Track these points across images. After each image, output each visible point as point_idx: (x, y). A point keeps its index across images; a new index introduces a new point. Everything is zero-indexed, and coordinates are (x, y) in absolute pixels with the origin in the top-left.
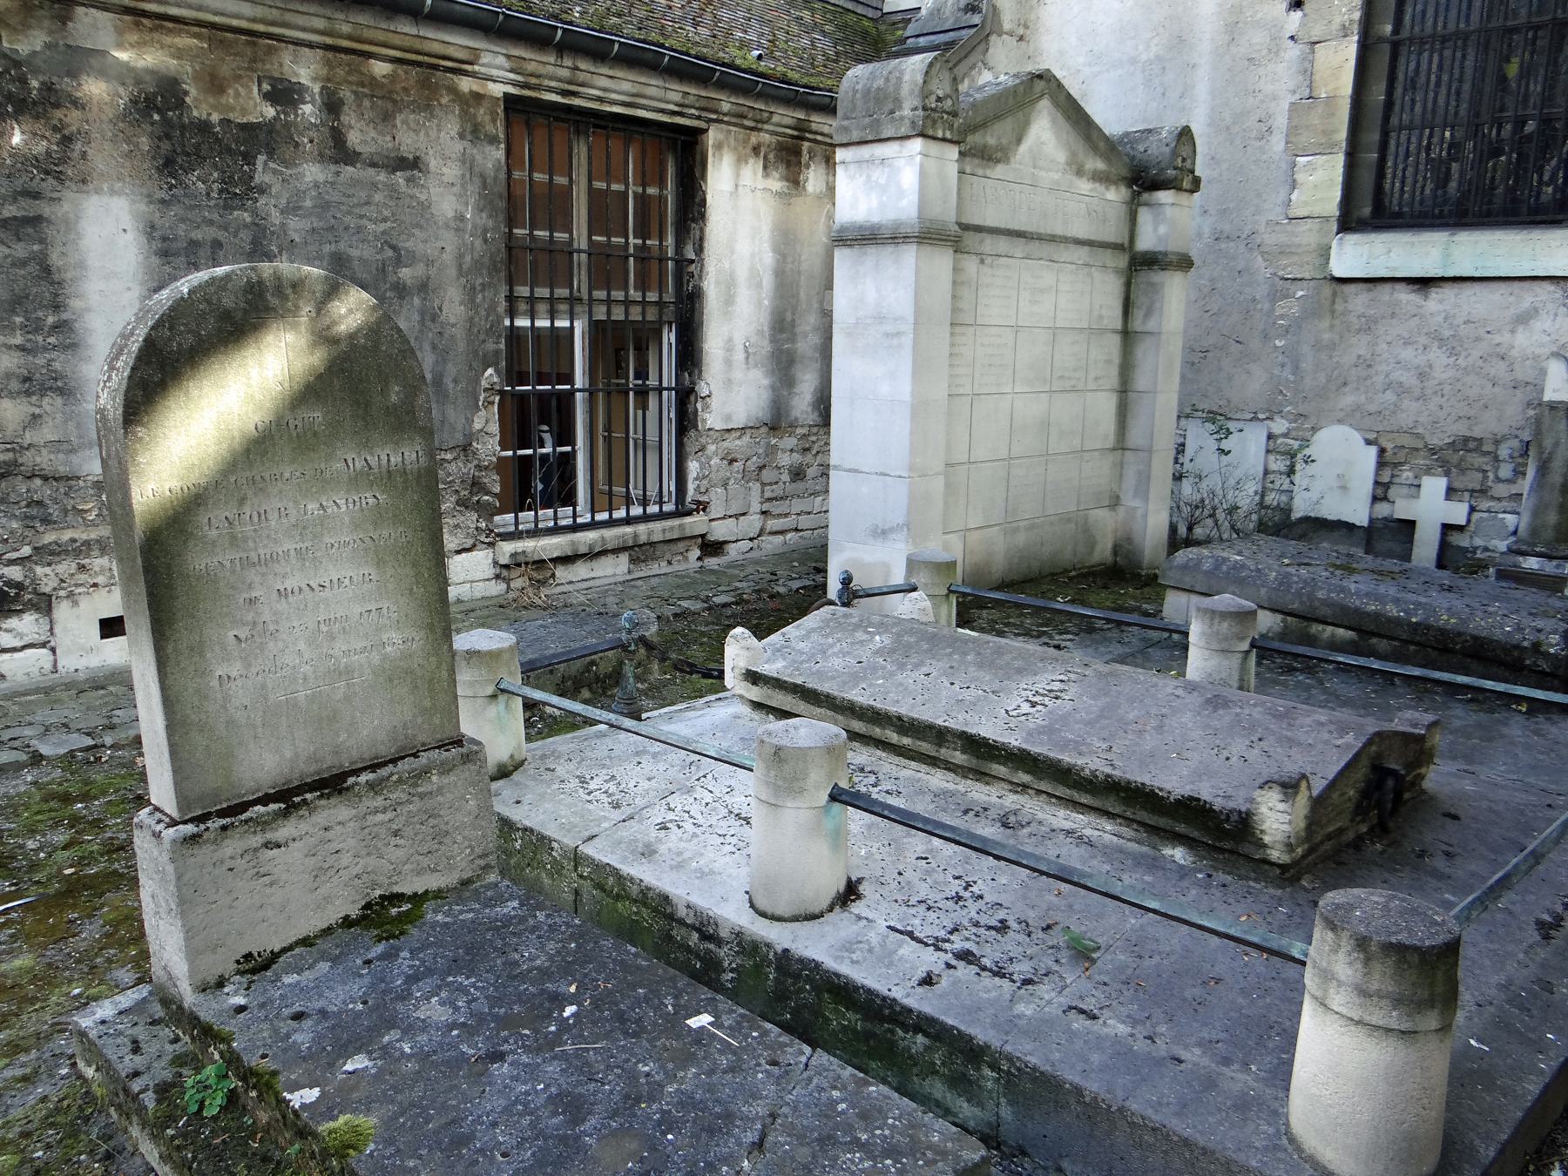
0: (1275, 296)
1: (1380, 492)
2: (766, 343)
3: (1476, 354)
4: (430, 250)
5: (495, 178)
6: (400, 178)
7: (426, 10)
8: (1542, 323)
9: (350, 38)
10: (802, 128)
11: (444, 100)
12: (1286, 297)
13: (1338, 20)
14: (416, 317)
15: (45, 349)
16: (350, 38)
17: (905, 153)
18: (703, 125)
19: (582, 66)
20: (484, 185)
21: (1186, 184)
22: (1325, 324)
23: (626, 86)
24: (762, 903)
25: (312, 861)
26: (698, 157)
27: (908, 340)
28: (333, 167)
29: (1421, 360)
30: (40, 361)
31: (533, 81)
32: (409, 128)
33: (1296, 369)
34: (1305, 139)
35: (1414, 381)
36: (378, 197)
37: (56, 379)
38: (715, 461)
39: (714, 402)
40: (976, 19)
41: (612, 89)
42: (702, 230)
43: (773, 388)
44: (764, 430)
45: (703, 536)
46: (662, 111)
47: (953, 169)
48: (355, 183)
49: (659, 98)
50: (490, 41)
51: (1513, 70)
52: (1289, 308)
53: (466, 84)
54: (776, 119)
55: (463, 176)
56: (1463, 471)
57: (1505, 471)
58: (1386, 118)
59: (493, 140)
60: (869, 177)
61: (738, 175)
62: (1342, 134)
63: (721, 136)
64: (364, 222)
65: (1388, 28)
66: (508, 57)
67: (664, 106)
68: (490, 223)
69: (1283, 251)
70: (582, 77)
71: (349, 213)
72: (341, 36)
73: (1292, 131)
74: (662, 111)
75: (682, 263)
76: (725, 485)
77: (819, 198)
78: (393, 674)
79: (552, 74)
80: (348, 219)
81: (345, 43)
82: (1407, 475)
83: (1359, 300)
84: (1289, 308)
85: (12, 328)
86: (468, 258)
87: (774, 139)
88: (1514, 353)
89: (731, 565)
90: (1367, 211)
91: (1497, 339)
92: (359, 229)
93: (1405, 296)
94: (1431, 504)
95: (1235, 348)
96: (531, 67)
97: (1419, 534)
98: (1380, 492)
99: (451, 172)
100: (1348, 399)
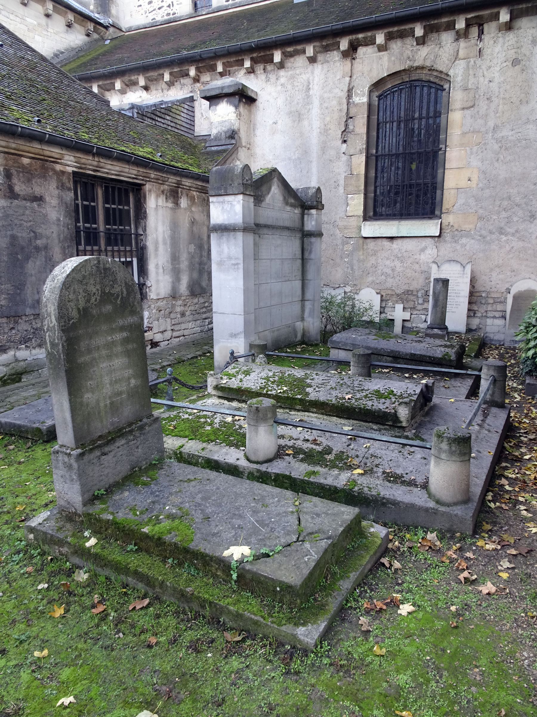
0: (344, 243)
1: (382, 310)
2: (170, 265)
3: (409, 262)
4: (48, 233)
5: (71, 204)
6: (35, 204)
7: (46, 139)
8: (429, 251)
9: (15, 149)
10: (179, 184)
11: (50, 174)
12: (348, 243)
13: (358, 148)
14: (44, 259)
16: (15, 149)
17: (237, 199)
18: (144, 183)
19: (102, 160)
20: (67, 207)
21: (320, 207)
22: (361, 253)
23: (117, 168)
24: (253, 458)
26: (142, 195)
27: (241, 266)
28: (10, 201)
29: (392, 265)
31: (83, 166)
32: (38, 185)
33: (352, 269)
34: (350, 188)
35: (391, 272)
36: (27, 212)
38: (154, 311)
39: (153, 289)
40: (233, 141)
41: (112, 169)
42: (145, 223)
43: (173, 282)
44: (171, 298)
45: (151, 340)
46: (130, 177)
47: (252, 205)
48: (18, 206)
49: (127, 173)
50: (69, 151)
51: (414, 167)
52: (348, 248)
53: (58, 167)
54: (170, 180)
55: (59, 204)
56: (407, 301)
57: (421, 301)
58: (376, 182)
59: (69, 189)
60: (223, 208)
61: (157, 202)
62: (362, 187)
63: (150, 187)
64: (22, 222)
65: (374, 151)
66: (74, 157)
67: (130, 176)
68: (70, 222)
69: (346, 228)
70: (102, 165)
71: (17, 219)
72: (11, 149)
73: (346, 186)
74: (130, 177)
75: (137, 235)
76: (158, 320)
77: (185, 209)
79: (90, 164)
80: (16, 221)
81: (13, 151)
82: (390, 304)
83: (371, 244)
84: (348, 248)
86: (62, 236)
87: (169, 188)
88: (421, 261)
89: (162, 350)
90: (371, 214)
91: (415, 257)
92: (21, 225)
93: (386, 243)
94: (399, 314)
95: (331, 262)
96: (83, 161)
97: (396, 323)
98: (382, 310)
99: (55, 202)
100: (370, 279)
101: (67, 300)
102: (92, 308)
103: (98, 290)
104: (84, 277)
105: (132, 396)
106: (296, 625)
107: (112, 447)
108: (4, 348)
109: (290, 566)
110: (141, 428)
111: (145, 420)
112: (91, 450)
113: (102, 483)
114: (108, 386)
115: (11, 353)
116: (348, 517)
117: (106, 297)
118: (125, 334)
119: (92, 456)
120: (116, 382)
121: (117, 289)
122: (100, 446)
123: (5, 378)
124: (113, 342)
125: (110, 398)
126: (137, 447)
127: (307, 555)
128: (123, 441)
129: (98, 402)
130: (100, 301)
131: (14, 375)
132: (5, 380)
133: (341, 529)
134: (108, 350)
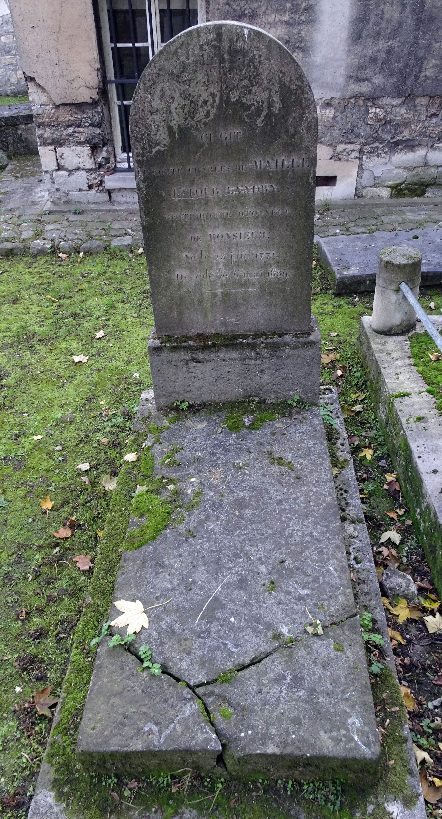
15: (299, 24)
25: (215, 373)
30: (295, 31)
37: (301, 42)
78: (269, 291)
85: (284, 11)
101: (147, 110)
102: (197, 129)
103: (213, 95)
104: (184, 67)
105: (270, 293)
106: (56, 784)
107: (212, 356)
108: (412, 143)
109: (121, 710)
110: (275, 347)
111: (287, 338)
112: (173, 349)
113: (189, 395)
114: (221, 266)
115: (421, 152)
116: (330, 744)
117: (230, 111)
118: (268, 187)
119: (174, 356)
120: (238, 264)
121: (258, 96)
122: (188, 348)
123: (402, 187)
124: (238, 197)
125: (223, 285)
126: (262, 371)
127: (157, 724)
128: (234, 355)
129: (199, 286)
130: (217, 117)
131: (416, 184)
132: (401, 190)
133: (271, 749)
134: (225, 208)
